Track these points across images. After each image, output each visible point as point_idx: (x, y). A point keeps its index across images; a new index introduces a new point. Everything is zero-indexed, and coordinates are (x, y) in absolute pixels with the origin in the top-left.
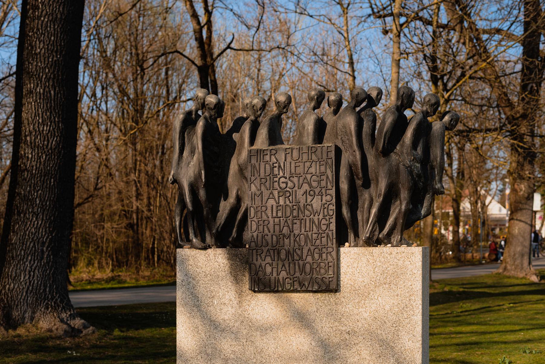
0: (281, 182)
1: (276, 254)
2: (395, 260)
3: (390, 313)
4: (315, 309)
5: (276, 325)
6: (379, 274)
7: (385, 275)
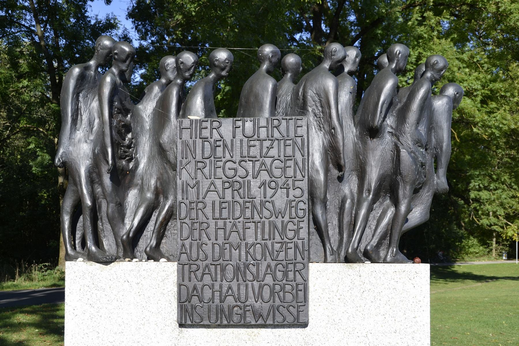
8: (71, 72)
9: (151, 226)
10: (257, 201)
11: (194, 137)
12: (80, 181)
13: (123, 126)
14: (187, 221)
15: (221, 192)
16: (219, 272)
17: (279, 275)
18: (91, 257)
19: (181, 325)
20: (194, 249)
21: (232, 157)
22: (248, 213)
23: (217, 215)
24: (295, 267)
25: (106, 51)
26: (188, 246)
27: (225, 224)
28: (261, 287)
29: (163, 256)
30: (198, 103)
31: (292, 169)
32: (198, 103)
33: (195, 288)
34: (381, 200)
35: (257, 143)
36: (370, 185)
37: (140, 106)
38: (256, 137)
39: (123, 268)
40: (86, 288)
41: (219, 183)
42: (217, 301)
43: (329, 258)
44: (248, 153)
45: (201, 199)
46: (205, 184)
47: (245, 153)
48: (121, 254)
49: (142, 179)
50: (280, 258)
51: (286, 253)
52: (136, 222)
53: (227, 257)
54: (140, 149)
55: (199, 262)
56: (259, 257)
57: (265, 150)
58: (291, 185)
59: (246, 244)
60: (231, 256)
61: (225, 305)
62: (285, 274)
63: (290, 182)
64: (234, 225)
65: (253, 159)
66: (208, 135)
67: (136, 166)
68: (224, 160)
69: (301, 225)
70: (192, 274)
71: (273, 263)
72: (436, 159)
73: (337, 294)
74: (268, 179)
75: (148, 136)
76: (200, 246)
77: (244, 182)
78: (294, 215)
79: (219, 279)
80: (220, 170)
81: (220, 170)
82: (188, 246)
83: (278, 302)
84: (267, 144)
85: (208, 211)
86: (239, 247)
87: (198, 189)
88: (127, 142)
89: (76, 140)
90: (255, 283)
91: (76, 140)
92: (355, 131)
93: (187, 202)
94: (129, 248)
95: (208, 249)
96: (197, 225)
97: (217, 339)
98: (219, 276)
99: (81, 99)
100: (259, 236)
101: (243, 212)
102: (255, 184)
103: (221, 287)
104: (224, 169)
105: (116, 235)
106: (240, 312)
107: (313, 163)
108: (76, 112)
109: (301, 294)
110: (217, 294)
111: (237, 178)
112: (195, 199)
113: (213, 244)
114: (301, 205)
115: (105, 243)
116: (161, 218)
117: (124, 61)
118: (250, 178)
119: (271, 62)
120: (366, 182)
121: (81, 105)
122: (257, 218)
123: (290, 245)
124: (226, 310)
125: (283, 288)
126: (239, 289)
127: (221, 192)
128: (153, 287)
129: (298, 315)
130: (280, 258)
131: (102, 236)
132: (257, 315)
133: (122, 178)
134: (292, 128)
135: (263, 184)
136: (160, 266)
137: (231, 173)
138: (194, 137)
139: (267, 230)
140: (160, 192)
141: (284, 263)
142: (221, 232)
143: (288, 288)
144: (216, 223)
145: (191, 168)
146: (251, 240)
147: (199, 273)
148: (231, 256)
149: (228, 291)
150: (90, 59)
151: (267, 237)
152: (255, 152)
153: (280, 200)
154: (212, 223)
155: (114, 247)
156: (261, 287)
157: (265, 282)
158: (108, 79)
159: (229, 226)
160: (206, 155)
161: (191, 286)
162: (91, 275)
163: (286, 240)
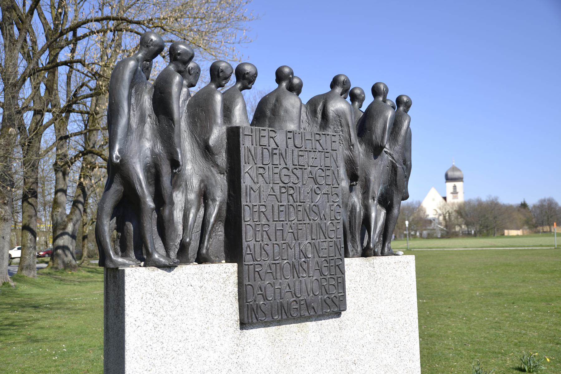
0: (283, 174)
1: (278, 270)
2: (394, 271)
3: (392, 332)
4: (319, 339)
5: (273, 368)
6: (380, 288)
7: (386, 288)
8: (128, 64)
11: (254, 144)
15: (278, 197)
21: (286, 165)
36: (374, 192)
39: (189, 271)
40: (149, 296)
73: (360, 284)
80: (277, 176)
81: (277, 176)
97: (273, 334)
116: (377, 232)
128: (216, 289)
136: (221, 268)
138: (254, 144)
162: (154, 282)
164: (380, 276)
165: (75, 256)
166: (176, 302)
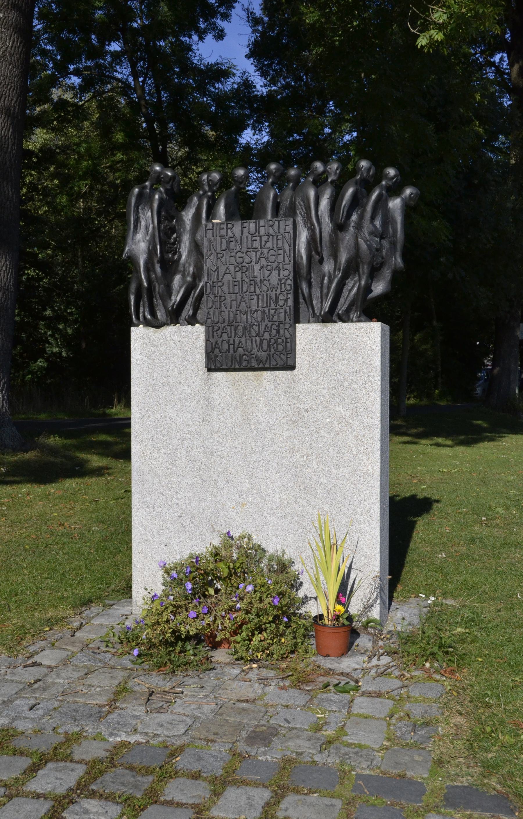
2: (354, 336)
4: (273, 387)
9: (190, 301)
10: (258, 280)
12: (140, 270)
13: (169, 229)
14: (211, 295)
16: (233, 331)
17: (274, 332)
18: (147, 323)
19: (209, 370)
20: (216, 314)
22: (252, 289)
23: (231, 291)
24: (284, 326)
25: (156, 175)
26: (211, 313)
27: (236, 297)
28: (261, 341)
29: (198, 322)
30: (222, 209)
31: (282, 256)
32: (222, 209)
33: (216, 343)
34: (351, 277)
35: (258, 238)
37: (183, 213)
38: (257, 234)
39: (170, 330)
40: (145, 346)
41: (232, 268)
42: (232, 351)
43: (311, 321)
44: (252, 246)
45: (220, 280)
46: (223, 269)
47: (250, 246)
48: (169, 322)
49: (184, 267)
50: (274, 320)
51: (279, 316)
52: (178, 299)
53: (238, 320)
54: (183, 245)
55: (219, 325)
56: (259, 319)
57: (263, 243)
58: (281, 268)
59: (251, 311)
60: (241, 319)
61: (237, 354)
62: (278, 331)
63: (281, 265)
64: (243, 297)
65: (255, 250)
66: (225, 234)
67: (180, 256)
68: (235, 251)
69: (289, 296)
70: (215, 333)
71: (269, 324)
72: (393, 244)
74: (265, 264)
75: (188, 235)
76: (220, 313)
77: (249, 267)
78: (283, 288)
79: (233, 336)
80: (233, 259)
81: (233, 259)
82: (211, 313)
83: (273, 351)
84: (265, 238)
85: (225, 288)
86: (246, 313)
87: (218, 272)
88: (172, 240)
89: (137, 241)
90: (257, 338)
91: (137, 241)
92: (331, 226)
93: (211, 282)
94: (175, 317)
95: (225, 315)
96: (217, 298)
98: (233, 334)
99: (140, 211)
100: (260, 305)
101: (248, 288)
102: (257, 267)
103: (234, 341)
104: (235, 258)
105: (165, 307)
106: (247, 359)
107: (299, 251)
108: (137, 221)
109: (289, 345)
110: (232, 346)
111: (244, 264)
112: (216, 280)
113: (229, 311)
114: (289, 282)
115: (159, 314)
116: (196, 295)
117: (168, 183)
118: (253, 263)
119: (274, 176)
120: (338, 264)
121: (141, 215)
122: (258, 292)
123: (281, 311)
124: (238, 357)
125: (276, 342)
126: (246, 342)
127: (233, 275)
129: (287, 360)
130: (274, 320)
131: (157, 309)
132: (259, 360)
133: (170, 267)
134: (282, 226)
135: (262, 267)
137: (241, 260)
139: (265, 300)
140: (197, 276)
141: (277, 323)
142: (234, 303)
143: (280, 341)
144: (231, 296)
145: (213, 258)
146: (254, 308)
147: (219, 332)
148: (241, 319)
149: (239, 345)
150: (146, 181)
151: (265, 305)
152: (257, 244)
153: (274, 279)
154: (228, 296)
155: (165, 317)
156: (261, 341)
157: (264, 337)
158: (157, 197)
159: (239, 298)
160: (224, 248)
161: (213, 341)
163: (278, 307)
164: (338, 340)
165: (330, 617)
166: (163, 351)
